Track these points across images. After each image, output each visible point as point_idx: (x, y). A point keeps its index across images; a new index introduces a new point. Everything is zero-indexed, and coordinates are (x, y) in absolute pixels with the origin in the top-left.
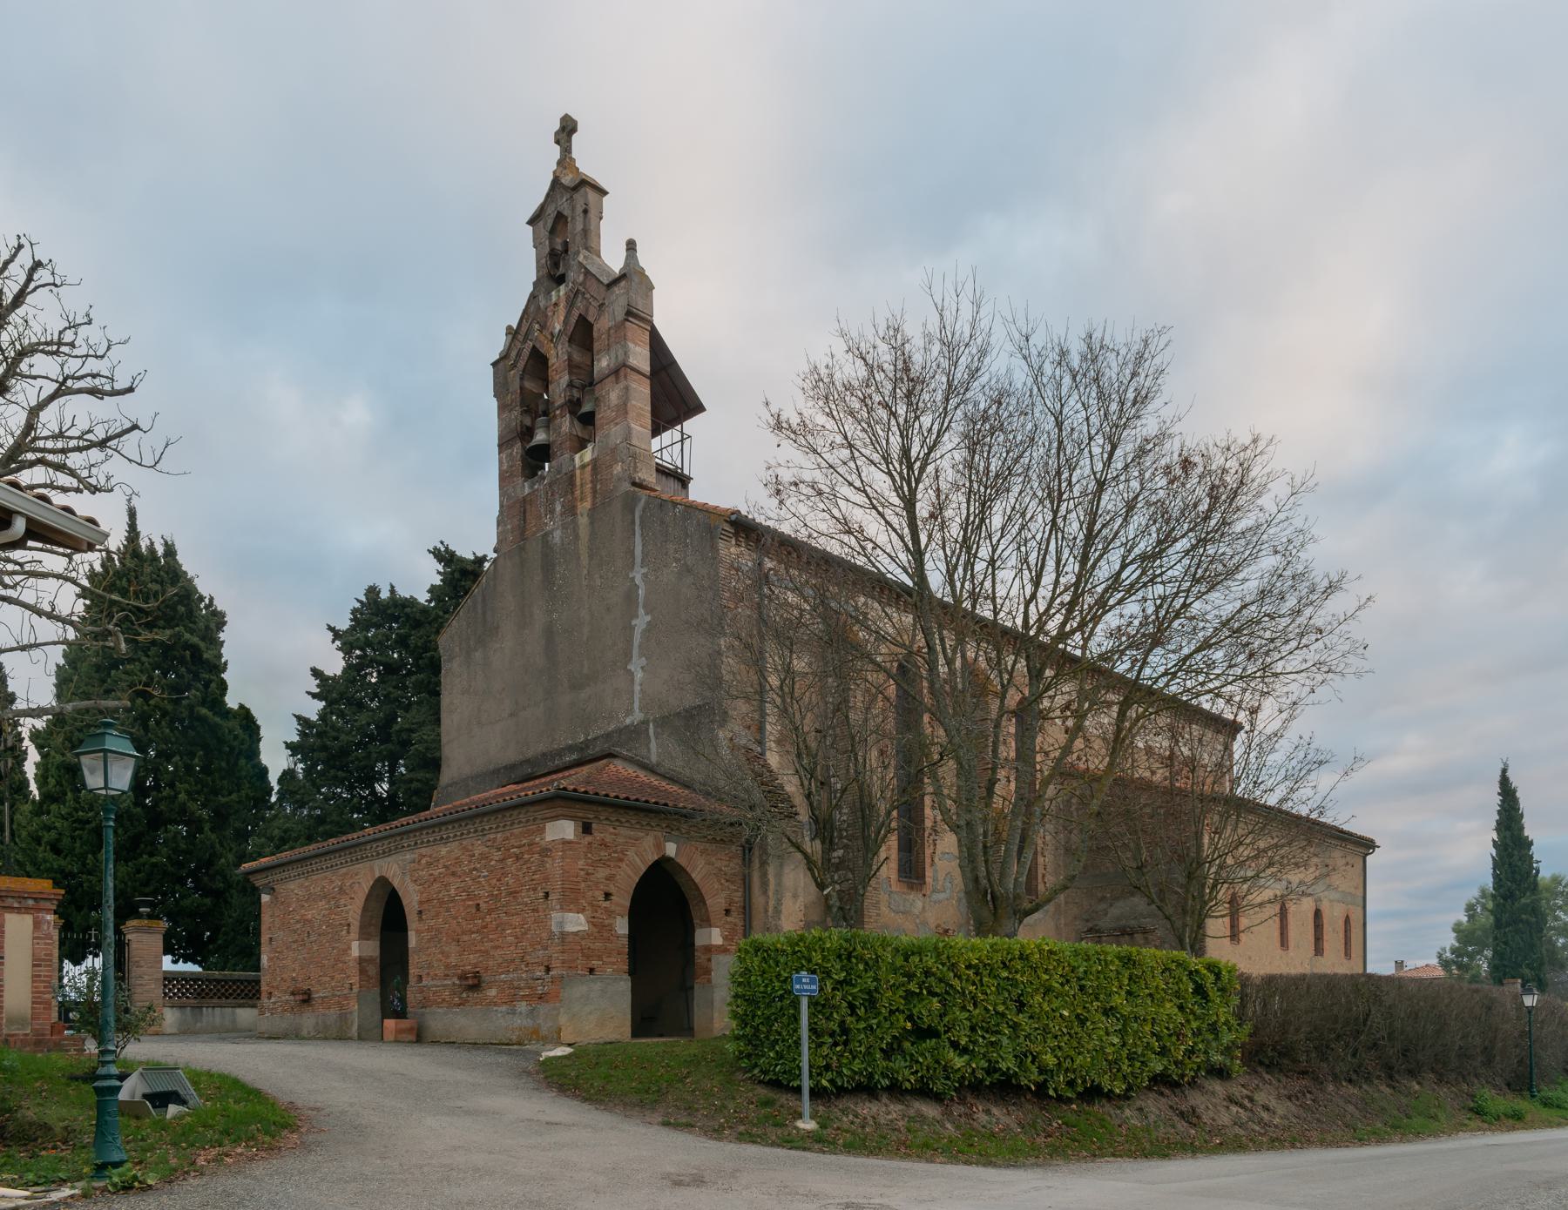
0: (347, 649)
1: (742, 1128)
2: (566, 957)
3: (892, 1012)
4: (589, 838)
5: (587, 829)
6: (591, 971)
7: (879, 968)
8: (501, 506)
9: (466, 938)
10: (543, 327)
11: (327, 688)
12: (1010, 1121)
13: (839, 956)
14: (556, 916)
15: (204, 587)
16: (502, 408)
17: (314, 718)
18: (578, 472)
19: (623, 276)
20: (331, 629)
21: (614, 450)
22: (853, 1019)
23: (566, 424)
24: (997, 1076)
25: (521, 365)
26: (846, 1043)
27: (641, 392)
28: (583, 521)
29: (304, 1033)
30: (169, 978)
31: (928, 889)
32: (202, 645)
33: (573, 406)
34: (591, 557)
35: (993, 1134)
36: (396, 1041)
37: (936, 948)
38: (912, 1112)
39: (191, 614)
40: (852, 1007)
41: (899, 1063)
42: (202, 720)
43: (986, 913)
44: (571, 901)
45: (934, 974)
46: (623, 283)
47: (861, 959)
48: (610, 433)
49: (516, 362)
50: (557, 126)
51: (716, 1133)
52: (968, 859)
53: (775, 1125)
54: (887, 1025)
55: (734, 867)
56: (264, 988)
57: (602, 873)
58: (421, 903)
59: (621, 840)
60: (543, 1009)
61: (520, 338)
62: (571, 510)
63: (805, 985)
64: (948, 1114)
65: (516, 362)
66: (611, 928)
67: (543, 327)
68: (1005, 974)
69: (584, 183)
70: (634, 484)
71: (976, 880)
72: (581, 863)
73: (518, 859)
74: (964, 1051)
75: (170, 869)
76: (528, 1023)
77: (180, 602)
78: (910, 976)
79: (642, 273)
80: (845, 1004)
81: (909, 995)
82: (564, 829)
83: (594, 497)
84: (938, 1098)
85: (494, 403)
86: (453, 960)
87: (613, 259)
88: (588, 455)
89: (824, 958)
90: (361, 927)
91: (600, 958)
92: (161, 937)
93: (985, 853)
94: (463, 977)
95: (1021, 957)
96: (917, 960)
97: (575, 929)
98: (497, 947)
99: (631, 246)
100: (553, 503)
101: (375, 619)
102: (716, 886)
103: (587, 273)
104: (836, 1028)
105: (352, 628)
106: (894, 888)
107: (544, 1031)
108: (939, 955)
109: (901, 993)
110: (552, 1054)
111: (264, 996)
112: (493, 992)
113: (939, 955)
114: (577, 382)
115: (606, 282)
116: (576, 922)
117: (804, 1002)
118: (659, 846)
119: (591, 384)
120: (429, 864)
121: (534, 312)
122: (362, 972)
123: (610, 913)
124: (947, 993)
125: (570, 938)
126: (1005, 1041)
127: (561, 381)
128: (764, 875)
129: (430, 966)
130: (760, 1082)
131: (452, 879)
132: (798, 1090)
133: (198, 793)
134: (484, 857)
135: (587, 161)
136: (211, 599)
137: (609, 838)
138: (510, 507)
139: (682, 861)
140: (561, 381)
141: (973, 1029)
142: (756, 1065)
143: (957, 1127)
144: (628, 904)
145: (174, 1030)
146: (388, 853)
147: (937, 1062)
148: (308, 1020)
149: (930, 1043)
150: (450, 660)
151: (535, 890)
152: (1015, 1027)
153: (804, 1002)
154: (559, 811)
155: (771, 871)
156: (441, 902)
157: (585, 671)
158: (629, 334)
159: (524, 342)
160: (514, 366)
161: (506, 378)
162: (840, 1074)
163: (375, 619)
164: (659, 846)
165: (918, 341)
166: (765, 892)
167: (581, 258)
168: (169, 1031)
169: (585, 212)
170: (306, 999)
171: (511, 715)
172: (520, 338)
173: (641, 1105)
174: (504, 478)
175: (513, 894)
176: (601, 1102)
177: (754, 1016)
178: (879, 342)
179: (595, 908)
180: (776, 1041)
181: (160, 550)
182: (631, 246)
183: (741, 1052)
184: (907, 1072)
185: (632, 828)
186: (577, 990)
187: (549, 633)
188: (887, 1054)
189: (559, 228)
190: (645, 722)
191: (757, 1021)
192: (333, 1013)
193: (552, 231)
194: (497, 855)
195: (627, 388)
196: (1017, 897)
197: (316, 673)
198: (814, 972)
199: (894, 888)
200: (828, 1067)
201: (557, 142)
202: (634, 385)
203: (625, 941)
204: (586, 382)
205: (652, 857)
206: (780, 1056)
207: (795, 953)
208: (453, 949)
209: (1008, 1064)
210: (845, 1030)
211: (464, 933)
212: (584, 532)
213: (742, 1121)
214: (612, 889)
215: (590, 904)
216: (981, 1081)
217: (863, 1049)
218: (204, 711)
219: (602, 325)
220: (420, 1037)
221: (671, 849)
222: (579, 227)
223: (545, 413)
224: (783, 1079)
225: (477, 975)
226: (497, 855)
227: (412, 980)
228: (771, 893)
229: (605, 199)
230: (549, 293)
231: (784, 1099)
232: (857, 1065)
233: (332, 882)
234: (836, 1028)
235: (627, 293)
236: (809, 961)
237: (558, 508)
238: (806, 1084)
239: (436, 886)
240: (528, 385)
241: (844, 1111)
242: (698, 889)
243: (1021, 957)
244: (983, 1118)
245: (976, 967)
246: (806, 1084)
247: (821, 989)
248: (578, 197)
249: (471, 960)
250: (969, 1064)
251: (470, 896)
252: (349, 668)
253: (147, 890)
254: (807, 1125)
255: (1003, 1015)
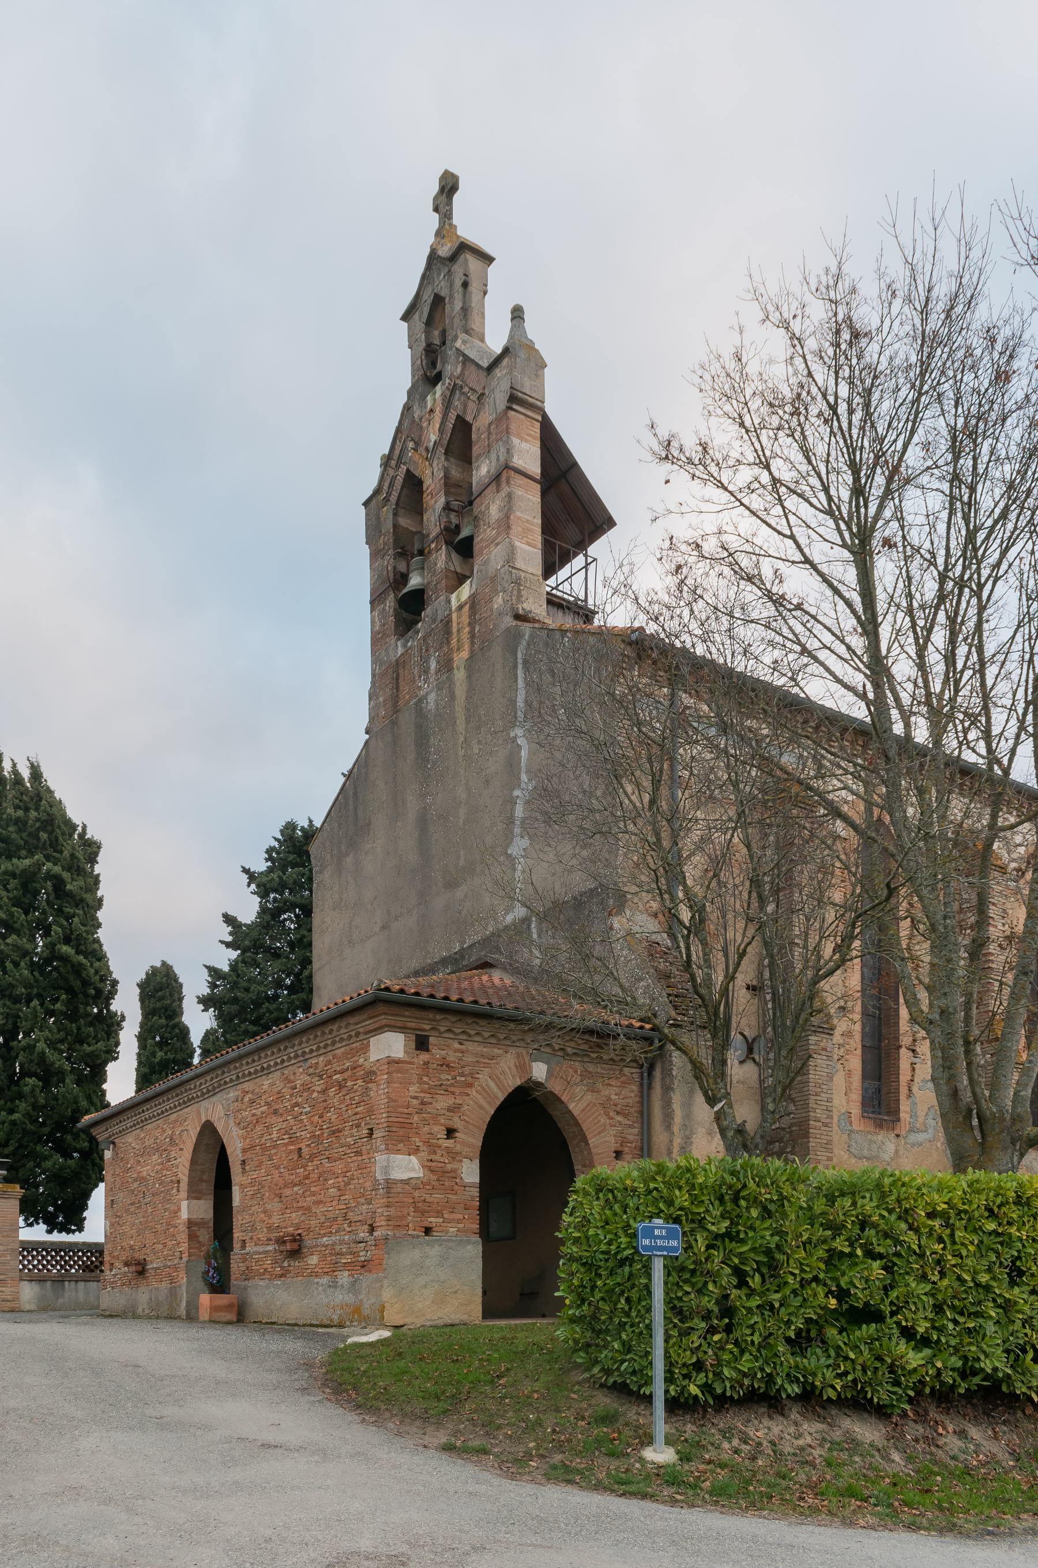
0: (263, 891)
1: (558, 1458)
2: (392, 1211)
3: (804, 1284)
4: (424, 1057)
5: (422, 1044)
6: (428, 1231)
7: (785, 1215)
8: (373, 675)
9: (287, 1192)
10: (417, 444)
11: (241, 936)
12: (998, 1449)
13: (721, 1199)
14: (381, 1159)
15: (75, 813)
16: (374, 555)
17: (226, 968)
18: (454, 616)
19: (506, 351)
20: (246, 871)
21: (493, 579)
22: (743, 1293)
23: (442, 558)
24: (977, 1380)
25: (394, 498)
26: (728, 1329)
27: (528, 503)
28: (460, 675)
29: (140, 1311)
30: (29, 1247)
31: (903, 1128)
32: (66, 875)
33: (450, 533)
34: (468, 720)
35: (968, 1471)
36: (212, 1321)
37: (879, 1185)
38: (837, 1435)
39: (55, 845)
40: (741, 1277)
41: (815, 1360)
42: (64, 959)
43: (970, 1142)
44: (400, 1137)
45: (875, 1226)
46: (505, 361)
47: (755, 1201)
48: (490, 557)
49: (389, 494)
50: (436, 188)
51: (514, 1467)
52: (945, 1065)
53: (611, 1454)
54: (797, 1302)
55: (630, 1093)
56: (107, 1258)
57: (442, 1103)
58: (244, 1151)
59: (469, 1059)
60: (367, 1279)
61: (393, 463)
62: (447, 666)
63: (659, 1239)
64: (896, 1438)
65: (389, 494)
66: (454, 1175)
67: (417, 444)
68: (991, 1226)
69: (464, 247)
70: (517, 617)
71: (955, 1094)
72: (413, 1089)
73: (341, 1087)
74: (925, 1342)
75: (29, 1126)
76: (350, 1299)
77: (43, 828)
78: (836, 1229)
79: (530, 347)
80: (728, 1270)
81: (833, 1258)
82: (391, 1045)
83: (472, 643)
84: (881, 1412)
85: (366, 550)
86: (275, 1220)
87: (496, 336)
88: (465, 591)
89: (695, 1200)
90: (191, 1184)
91: (439, 1214)
92: (18, 1203)
93: (968, 1052)
94: (281, 1241)
95: (1019, 1201)
96: (847, 1202)
97: (405, 1176)
98: (318, 1203)
99: (517, 314)
100: (427, 661)
101: (291, 857)
102: (603, 1119)
103: (467, 359)
104: (712, 1306)
105: (270, 870)
106: (856, 1127)
107: (366, 1312)
108: (883, 1196)
109: (821, 1253)
110: (364, 1339)
111: (105, 1267)
112: (313, 1260)
113: (883, 1196)
114: (455, 504)
115: (485, 364)
116: (406, 1167)
117: (658, 1268)
118: (523, 1068)
119: (471, 503)
120: (252, 1102)
121: (408, 429)
122: (192, 1237)
123: (454, 1156)
124: (897, 1254)
125: (398, 1188)
126: (990, 1328)
127: (435, 502)
128: (667, 1104)
129: (253, 1229)
130: (603, 1386)
131: (274, 1119)
132: (649, 1399)
133: (62, 1041)
134: (307, 1088)
135: (468, 226)
136: (84, 827)
137: (452, 1057)
138: (383, 675)
139: (556, 1087)
140: (435, 502)
141: (938, 1309)
142: (596, 1362)
143: (909, 1459)
144: (479, 1143)
145: (33, 1307)
146: (212, 1092)
147: (879, 1358)
148: (143, 1296)
149: (869, 1330)
150: (321, 872)
151: (358, 1126)
152: (1007, 1307)
153: (658, 1268)
154: (383, 1020)
155: (677, 1099)
156: (265, 1149)
157: (462, 863)
158: (513, 427)
159: (398, 466)
160: (387, 500)
161: (378, 518)
162: (718, 1375)
163: (291, 857)
164: (523, 1068)
165: (870, 289)
166: (668, 1127)
167: (458, 344)
168: (28, 1307)
169: (465, 285)
170: (141, 1270)
171: (383, 928)
172: (393, 463)
173: (424, 1418)
174: (377, 640)
175: (336, 1132)
176: (373, 1410)
177: (594, 1287)
178: (809, 298)
179: (433, 1148)
180: (622, 1325)
181: (25, 773)
182: (517, 314)
183: (576, 1341)
184: (829, 1374)
185: (485, 1043)
186: (409, 1256)
187: (423, 822)
188: (799, 1343)
189: (438, 316)
190: (526, 920)
191: (598, 1295)
192: (165, 1286)
193: (429, 323)
194: (319, 1085)
195: (510, 496)
196: (1016, 1119)
197: (229, 919)
198: (677, 1220)
199: (856, 1127)
200: (699, 1366)
201: (436, 209)
202: (519, 492)
203: (475, 1192)
204: (463, 500)
205: (513, 1082)
206: (627, 1348)
207: (649, 1192)
208: (274, 1206)
209: (995, 1362)
210: (727, 1311)
211: (286, 1186)
212: (460, 691)
213: (560, 1447)
214: (457, 1123)
215: (427, 1143)
216: (953, 1387)
217: (757, 1339)
218: (66, 949)
219: (482, 421)
220: (240, 1316)
221: (539, 1071)
222: (458, 305)
223: (421, 553)
224: (632, 1382)
225: (297, 1239)
226: (319, 1085)
227: (237, 1245)
228: (676, 1129)
229: (492, 270)
230: (423, 399)
231: (632, 1413)
232: (746, 1364)
233: (164, 1131)
234: (712, 1306)
235: (510, 373)
236: (670, 1203)
237: (433, 665)
238: (658, 1389)
239: (259, 1128)
240: (404, 522)
241: (727, 1434)
242: (577, 1124)
243: (1019, 1201)
244: (953, 1443)
245: (944, 1215)
246: (658, 1389)
247: (688, 1248)
248: (458, 269)
249: (291, 1221)
250: (930, 1362)
251: (293, 1139)
252: (263, 910)
253: (7, 1151)
254: (660, 1455)
255: (987, 1288)
